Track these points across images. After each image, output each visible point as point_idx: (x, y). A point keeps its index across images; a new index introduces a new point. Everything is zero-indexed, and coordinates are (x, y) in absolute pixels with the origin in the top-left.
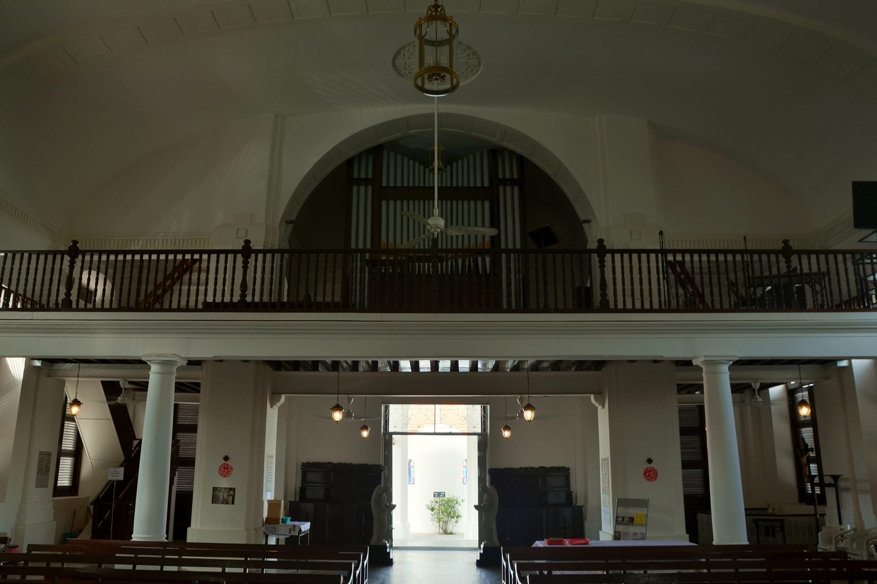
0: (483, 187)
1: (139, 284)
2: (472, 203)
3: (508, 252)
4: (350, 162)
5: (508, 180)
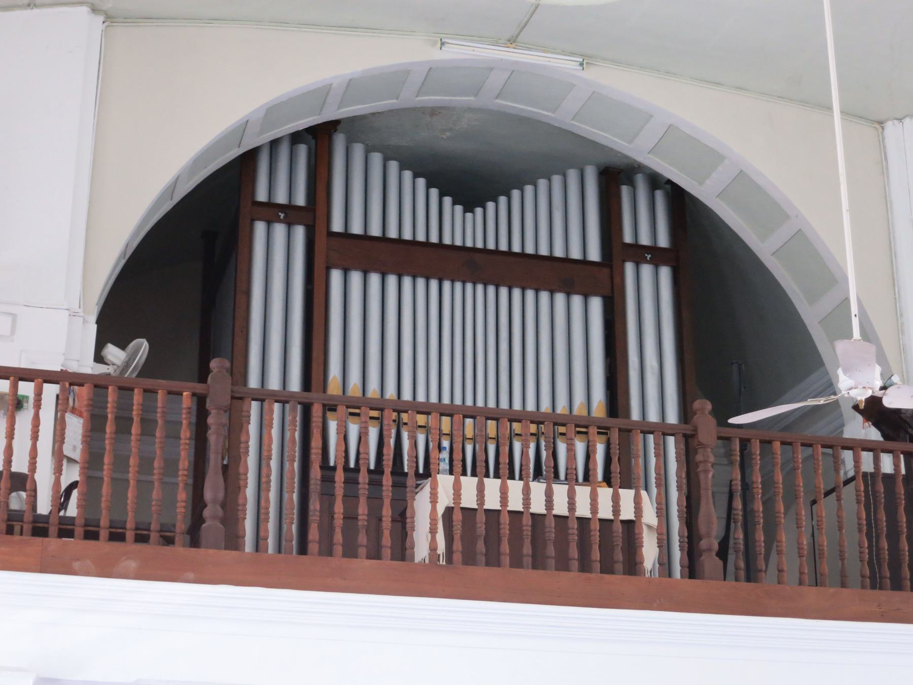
0: (584, 262)
1: (350, 517)
2: (517, 293)
3: (263, 396)
4: (249, 159)
5: (281, 207)
